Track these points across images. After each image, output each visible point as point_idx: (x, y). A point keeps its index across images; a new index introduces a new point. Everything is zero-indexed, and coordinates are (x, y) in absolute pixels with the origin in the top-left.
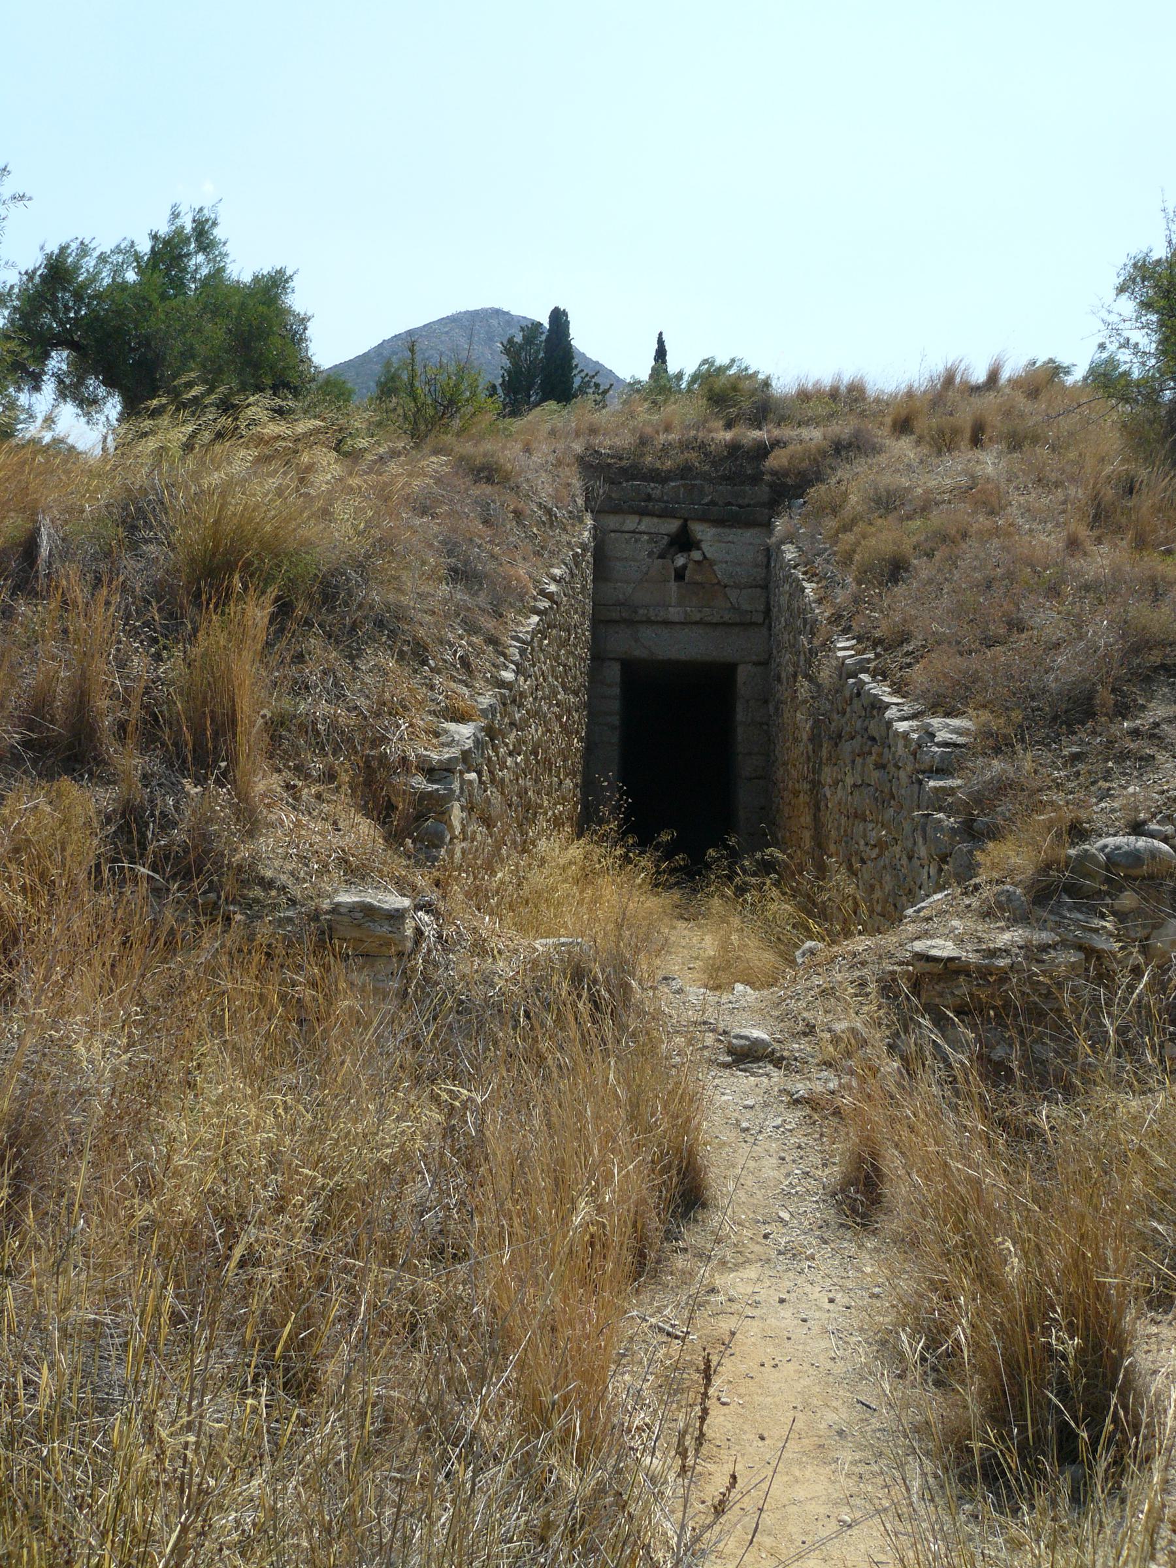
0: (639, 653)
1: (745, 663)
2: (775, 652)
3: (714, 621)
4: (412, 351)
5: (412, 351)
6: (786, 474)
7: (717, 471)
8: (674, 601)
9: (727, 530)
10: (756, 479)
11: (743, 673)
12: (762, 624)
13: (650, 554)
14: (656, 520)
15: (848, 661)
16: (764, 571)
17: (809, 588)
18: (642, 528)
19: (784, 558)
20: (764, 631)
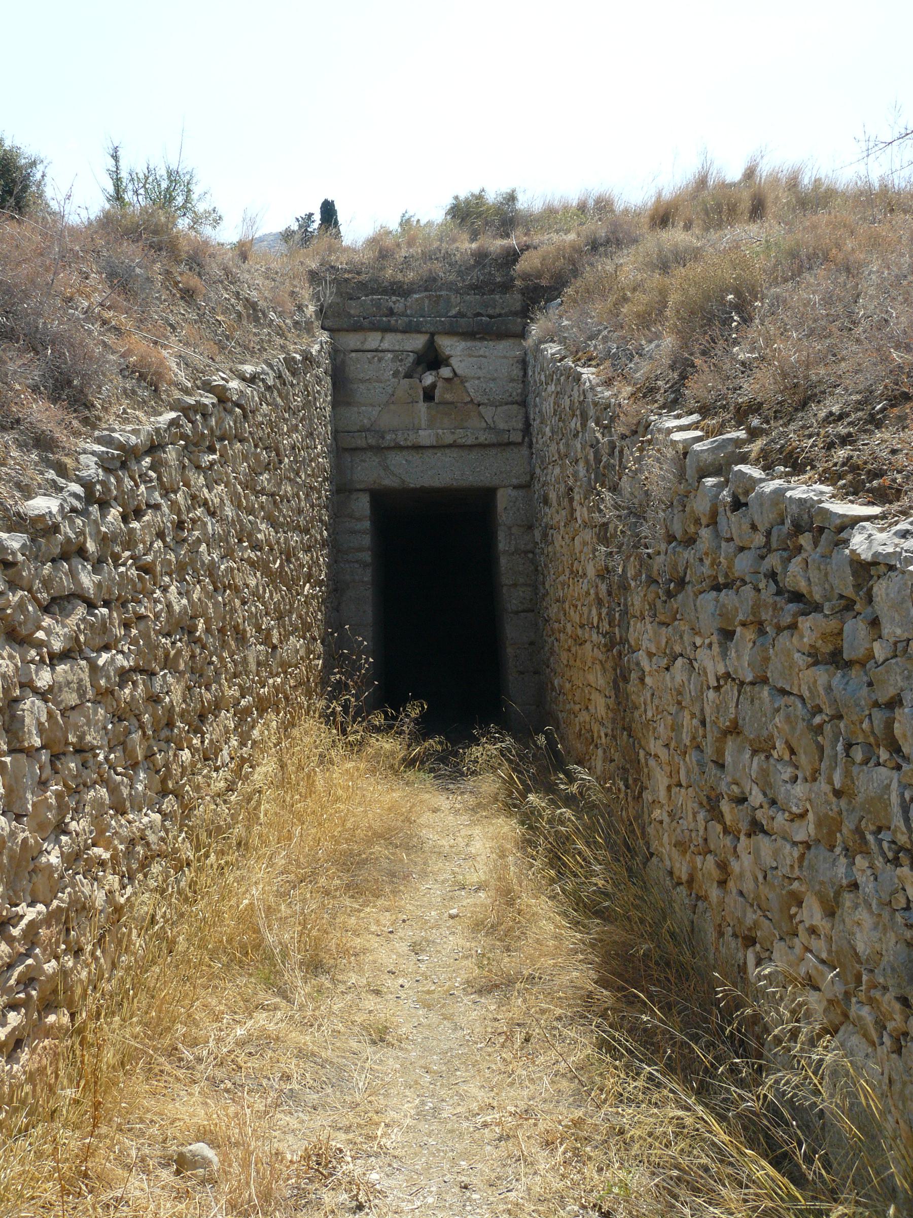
0: (389, 482)
1: (505, 487)
2: (538, 471)
3: (469, 442)
4: (115, 158)
5: (115, 158)
6: (539, 276)
7: (464, 281)
8: (423, 424)
9: (478, 344)
10: (506, 287)
11: (503, 498)
12: (520, 444)
13: (396, 374)
14: (399, 336)
15: (697, 447)
16: (521, 386)
17: (588, 374)
18: (385, 345)
19: (544, 357)
20: (525, 451)
